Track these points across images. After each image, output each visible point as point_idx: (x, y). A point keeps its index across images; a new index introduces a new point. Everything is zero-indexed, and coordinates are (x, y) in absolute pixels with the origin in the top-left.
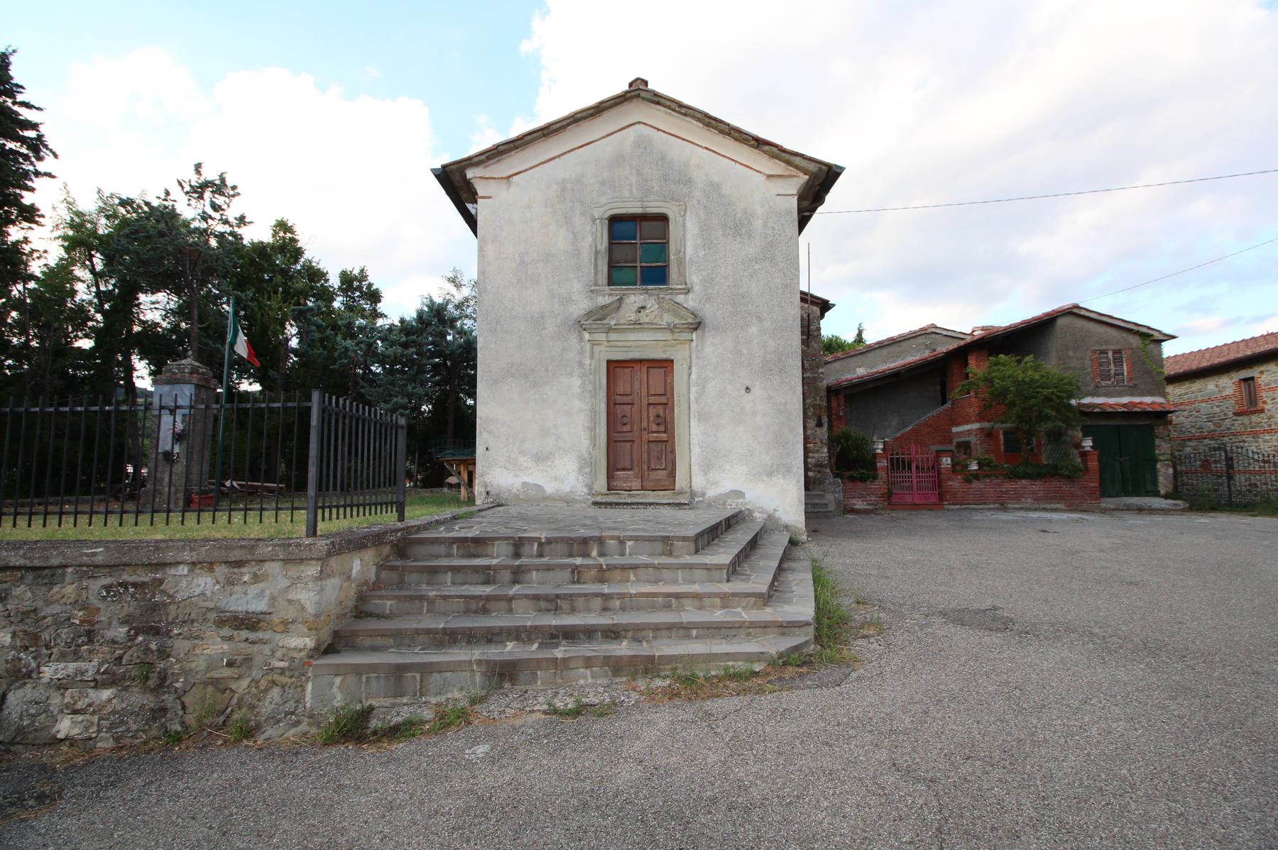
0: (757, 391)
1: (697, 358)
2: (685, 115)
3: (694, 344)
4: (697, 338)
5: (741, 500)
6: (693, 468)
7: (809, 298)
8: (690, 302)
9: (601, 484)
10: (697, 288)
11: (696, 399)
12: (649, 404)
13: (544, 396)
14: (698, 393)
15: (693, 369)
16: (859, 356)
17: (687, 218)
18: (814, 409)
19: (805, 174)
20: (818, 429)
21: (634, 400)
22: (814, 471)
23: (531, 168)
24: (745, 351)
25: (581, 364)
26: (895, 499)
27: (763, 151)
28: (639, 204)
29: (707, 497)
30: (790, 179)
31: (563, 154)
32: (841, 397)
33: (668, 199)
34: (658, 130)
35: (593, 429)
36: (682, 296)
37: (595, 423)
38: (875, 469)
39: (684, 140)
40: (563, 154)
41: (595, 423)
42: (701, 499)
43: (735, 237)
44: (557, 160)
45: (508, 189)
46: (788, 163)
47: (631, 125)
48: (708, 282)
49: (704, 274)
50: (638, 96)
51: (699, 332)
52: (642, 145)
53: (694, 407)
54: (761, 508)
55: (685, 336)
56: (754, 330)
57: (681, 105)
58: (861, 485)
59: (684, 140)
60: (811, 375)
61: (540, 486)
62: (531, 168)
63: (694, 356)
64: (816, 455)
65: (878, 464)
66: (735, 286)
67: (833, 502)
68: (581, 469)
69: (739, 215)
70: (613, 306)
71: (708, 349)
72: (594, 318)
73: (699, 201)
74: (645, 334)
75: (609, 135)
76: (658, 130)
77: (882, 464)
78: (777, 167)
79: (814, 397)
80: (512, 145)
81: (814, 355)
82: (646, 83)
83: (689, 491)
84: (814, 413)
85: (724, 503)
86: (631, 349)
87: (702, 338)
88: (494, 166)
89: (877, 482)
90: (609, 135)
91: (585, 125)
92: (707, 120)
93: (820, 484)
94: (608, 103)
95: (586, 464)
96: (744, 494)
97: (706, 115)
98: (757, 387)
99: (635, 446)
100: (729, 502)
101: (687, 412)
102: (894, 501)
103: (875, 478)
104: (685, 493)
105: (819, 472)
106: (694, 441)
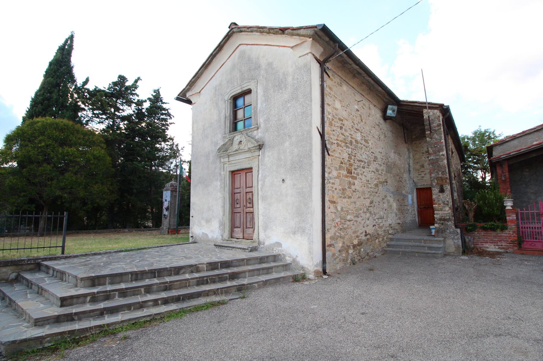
0: (288, 181)
1: (262, 165)
2: (252, 32)
3: (260, 157)
4: (262, 153)
5: (280, 248)
6: (260, 228)
7: (427, 105)
8: (258, 134)
9: (226, 235)
10: (262, 125)
11: (261, 188)
12: (246, 193)
13: (209, 191)
14: (262, 185)
15: (260, 172)
16: (535, 133)
17: (258, 88)
18: (437, 180)
19: (310, 38)
20: (440, 194)
21: (240, 190)
22: (439, 223)
23: (206, 85)
24: (283, 158)
25: (220, 174)
26: (525, 245)
27: (287, 34)
28: (240, 88)
29: (265, 245)
30: (303, 45)
31: (215, 74)
32: (506, 168)
33: (250, 80)
34: (247, 45)
35: (224, 207)
36: (256, 132)
37: (224, 204)
38: (506, 221)
39: (257, 45)
40: (215, 74)
41: (224, 204)
42: (263, 246)
43: (279, 91)
44: (214, 77)
45: (200, 97)
46: (299, 35)
47: (237, 48)
48: (267, 120)
49: (265, 116)
50: (234, 32)
51: (262, 150)
52: (242, 55)
53: (260, 193)
54: (290, 254)
55: (257, 153)
56: (287, 144)
57: (249, 28)
58: (493, 234)
59: (257, 45)
60: (434, 158)
61: (207, 235)
62: (206, 85)
63: (260, 164)
64: (440, 212)
65: (507, 218)
66: (278, 120)
67: (453, 246)
68: (220, 226)
69: (281, 77)
70: (228, 143)
71: (266, 159)
72: (222, 151)
73: (263, 76)
74: (242, 155)
75: (229, 57)
76: (247, 45)
77: (511, 218)
78: (293, 41)
79: (437, 172)
80: (196, 78)
81: (436, 143)
82: (235, 24)
83: (258, 241)
84: (437, 184)
85: (273, 249)
86: (237, 164)
87: (264, 154)
88: (194, 89)
89: (507, 232)
90: (229, 57)
91: (218, 56)
92: (259, 29)
93: (442, 232)
94: (223, 42)
95: (222, 224)
96: (282, 244)
97: (259, 28)
98: (288, 179)
99: (242, 214)
100: (275, 249)
101: (257, 196)
102: (525, 246)
103: (503, 229)
104: (256, 242)
105: (442, 224)
106: (260, 213)
